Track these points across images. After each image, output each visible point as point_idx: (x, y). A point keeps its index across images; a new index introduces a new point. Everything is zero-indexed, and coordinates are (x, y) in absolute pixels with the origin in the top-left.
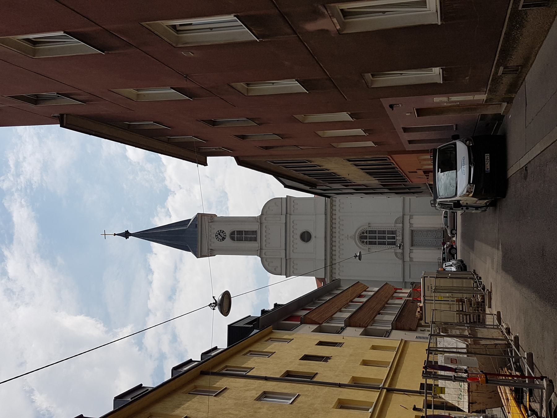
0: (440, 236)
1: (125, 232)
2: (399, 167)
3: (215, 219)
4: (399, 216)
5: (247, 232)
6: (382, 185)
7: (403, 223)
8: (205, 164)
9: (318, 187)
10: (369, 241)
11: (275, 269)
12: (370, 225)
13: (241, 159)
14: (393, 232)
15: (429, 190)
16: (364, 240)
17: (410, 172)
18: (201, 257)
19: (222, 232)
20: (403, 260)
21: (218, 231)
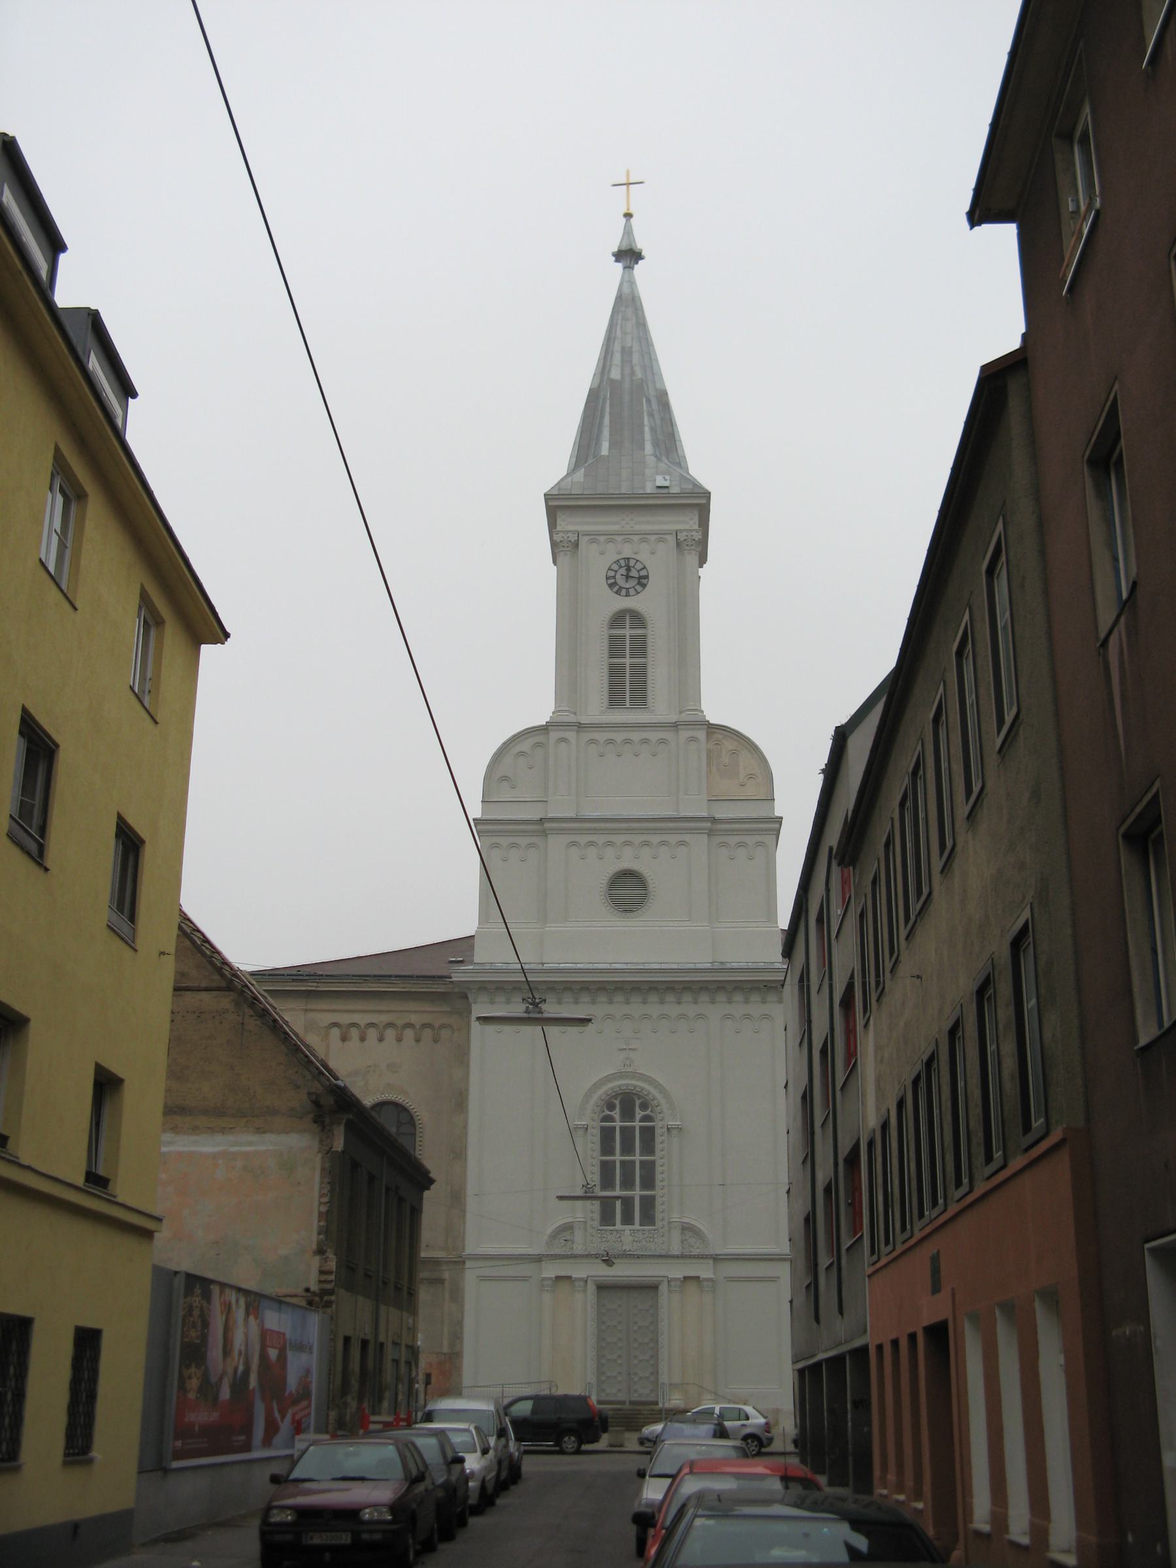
2: (998, 1187)
3: (692, 558)
5: (640, 673)
6: (856, 1148)
7: (682, 1256)
8: (979, 213)
9: (836, 870)
10: (614, 1128)
11: (505, 778)
12: (674, 1132)
13: (1014, 387)
14: (648, 1217)
15: (826, 1350)
16: (617, 1110)
17: (935, 1260)
18: (548, 507)
21: (645, 568)
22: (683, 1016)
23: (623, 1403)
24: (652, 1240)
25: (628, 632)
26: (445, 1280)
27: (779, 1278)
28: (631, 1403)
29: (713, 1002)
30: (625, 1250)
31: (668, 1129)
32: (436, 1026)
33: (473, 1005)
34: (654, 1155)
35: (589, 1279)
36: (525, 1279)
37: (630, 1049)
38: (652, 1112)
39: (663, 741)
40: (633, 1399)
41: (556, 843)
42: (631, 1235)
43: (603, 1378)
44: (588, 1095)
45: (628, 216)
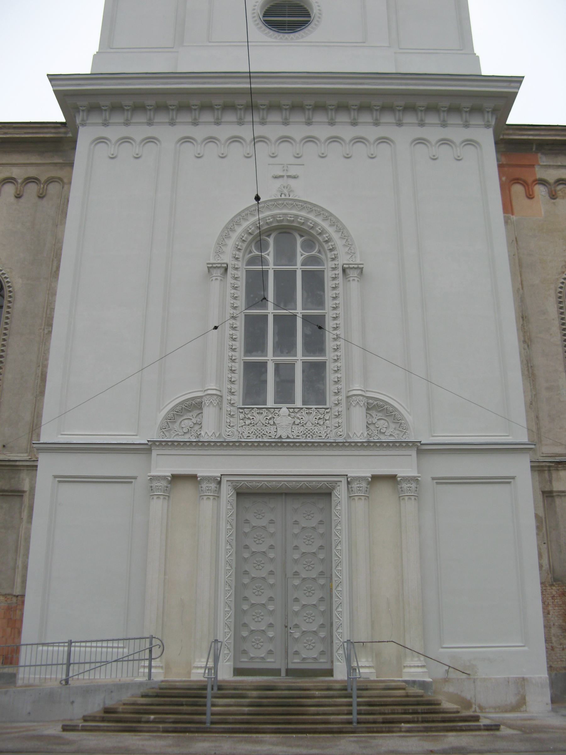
0: (296, 653)
4: (409, 418)
7: (368, 445)
12: (353, 274)
22: (359, 140)
23: (276, 672)
24: (322, 423)
26: (24, 492)
27: (513, 478)
28: (289, 672)
29: (400, 124)
30: (280, 437)
31: (344, 270)
32: (43, 179)
33: (80, 127)
34: (324, 309)
35: (224, 479)
36: (126, 480)
37: (289, 177)
38: (319, 252)
40: (291, 666)
42: (289, 415)
43: (245, 634)
44: (229, 228)
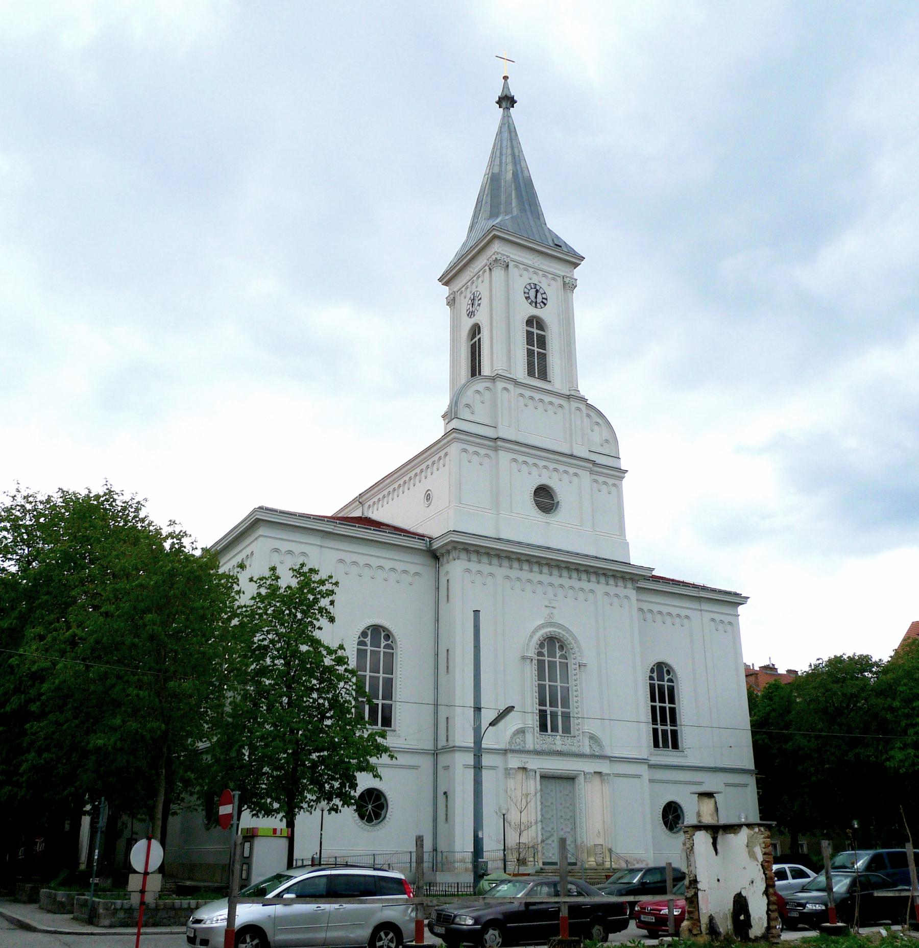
1: (512, 94)
5: (543, 357)
7: (593, 756)
14: (567, 730)
19: (544, 300)
20: (513, 751)
25: (535, 331)
39: (561, 406)
41: (504, 457)
45: (506, 78)
